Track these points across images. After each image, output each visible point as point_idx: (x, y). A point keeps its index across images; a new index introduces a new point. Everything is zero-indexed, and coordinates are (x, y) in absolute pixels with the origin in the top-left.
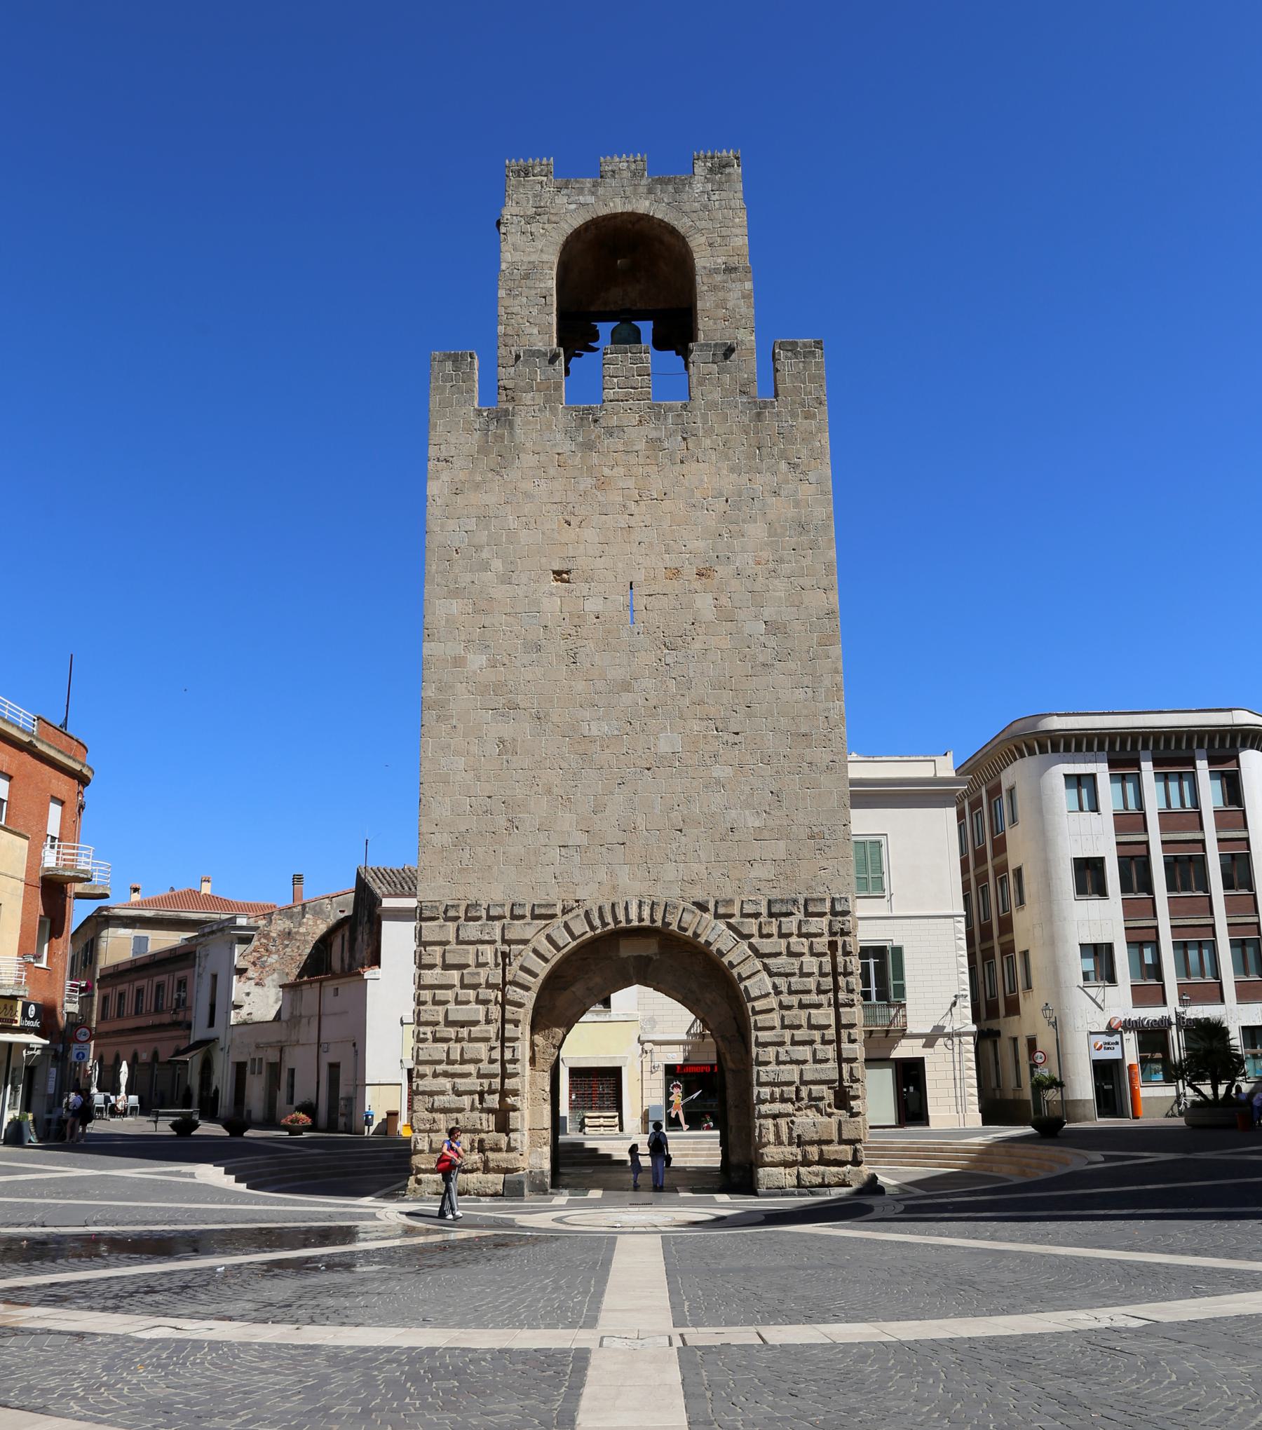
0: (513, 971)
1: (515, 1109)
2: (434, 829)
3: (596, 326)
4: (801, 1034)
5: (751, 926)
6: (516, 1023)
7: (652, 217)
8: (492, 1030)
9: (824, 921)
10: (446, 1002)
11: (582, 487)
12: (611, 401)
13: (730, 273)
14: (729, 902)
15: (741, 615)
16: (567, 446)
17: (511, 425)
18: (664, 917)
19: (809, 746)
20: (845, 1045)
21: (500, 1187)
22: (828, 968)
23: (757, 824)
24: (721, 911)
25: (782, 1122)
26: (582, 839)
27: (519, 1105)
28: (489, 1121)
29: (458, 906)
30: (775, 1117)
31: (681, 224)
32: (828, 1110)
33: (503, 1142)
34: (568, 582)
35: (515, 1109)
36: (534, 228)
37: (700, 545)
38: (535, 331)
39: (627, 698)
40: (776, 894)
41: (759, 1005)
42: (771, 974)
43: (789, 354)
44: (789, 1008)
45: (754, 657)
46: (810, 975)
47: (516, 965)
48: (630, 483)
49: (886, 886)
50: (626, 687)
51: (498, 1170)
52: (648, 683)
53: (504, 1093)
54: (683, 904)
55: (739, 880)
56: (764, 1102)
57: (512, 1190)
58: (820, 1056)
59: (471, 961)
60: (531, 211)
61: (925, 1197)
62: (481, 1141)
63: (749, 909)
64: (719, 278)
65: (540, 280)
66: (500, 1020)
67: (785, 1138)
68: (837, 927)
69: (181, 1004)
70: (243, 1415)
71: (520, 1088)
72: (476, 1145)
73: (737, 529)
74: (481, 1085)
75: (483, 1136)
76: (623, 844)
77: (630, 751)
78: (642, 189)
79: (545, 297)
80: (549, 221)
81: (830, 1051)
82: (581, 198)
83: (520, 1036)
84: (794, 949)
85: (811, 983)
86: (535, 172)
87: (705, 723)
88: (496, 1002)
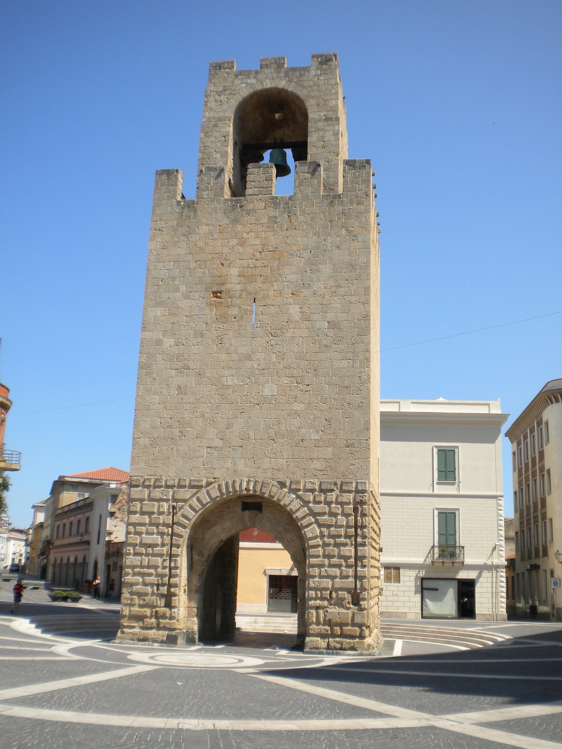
0: (179, 518)
1: (175, 595)
2: (141, 435)
4: (335, 560)
5: (310, 497)
6: (178, 546)
8: (165, 550)
9: (352, 495)
10: (142, 533)
11: (231, 244)
12: (250, 195)
14: (298, 482)
15: (315, 317)
16: (226, 221)
18: (261, 489)
19: (349, 394)
20: (359, 569)
21: (165, 638)
22: (352, 523)
24: (293, 486)
25: (321, 612)
26: (218, 443)
27: (177, 592)
29: (150, 479)
30: (317, 608)
31: (302, 93)
32: (348, 605)
33: (168, 613)
34: (220, 298)
35: (175, 595)
36: (223, 98)
37: (293, 277)
39: (248, 364)
40: (325, 479)
41: (311, 543)
43: (351, 167)
44: (328, 545)
45: (320, 341)
46: (341, 526)
47: (179, 514)
48: (258, 242)
49: (457, 477)
50: (248, 357)
51: (165, 628)
52: (261, 356)
53: (170, 586)
55: (304, 469)
56: (312, 599)
57: (171, 640)
58: (344, 573)
59: (156, 511)
60: (221, 89)
62: (156, 612)
63: (309, 486)
64: (321, 124)
65: (223, 127)
66: (169, 544)
67: (322, 620)
68: (358, 499)
69: (87, 532)
71: (178, 583)
72: (154, 614)
73: (316, 268)
74: (158, 580)
75: (158, 609)
76: (241, 447)
77: (248, 394)
78: (282, 74)
79: (225, 137)
80: (230, 94)
81: (351, 572)
83: (180, 553)
84: (334, 510)
85: (342, 531)
87: (291, 379)
88: (168, 535)
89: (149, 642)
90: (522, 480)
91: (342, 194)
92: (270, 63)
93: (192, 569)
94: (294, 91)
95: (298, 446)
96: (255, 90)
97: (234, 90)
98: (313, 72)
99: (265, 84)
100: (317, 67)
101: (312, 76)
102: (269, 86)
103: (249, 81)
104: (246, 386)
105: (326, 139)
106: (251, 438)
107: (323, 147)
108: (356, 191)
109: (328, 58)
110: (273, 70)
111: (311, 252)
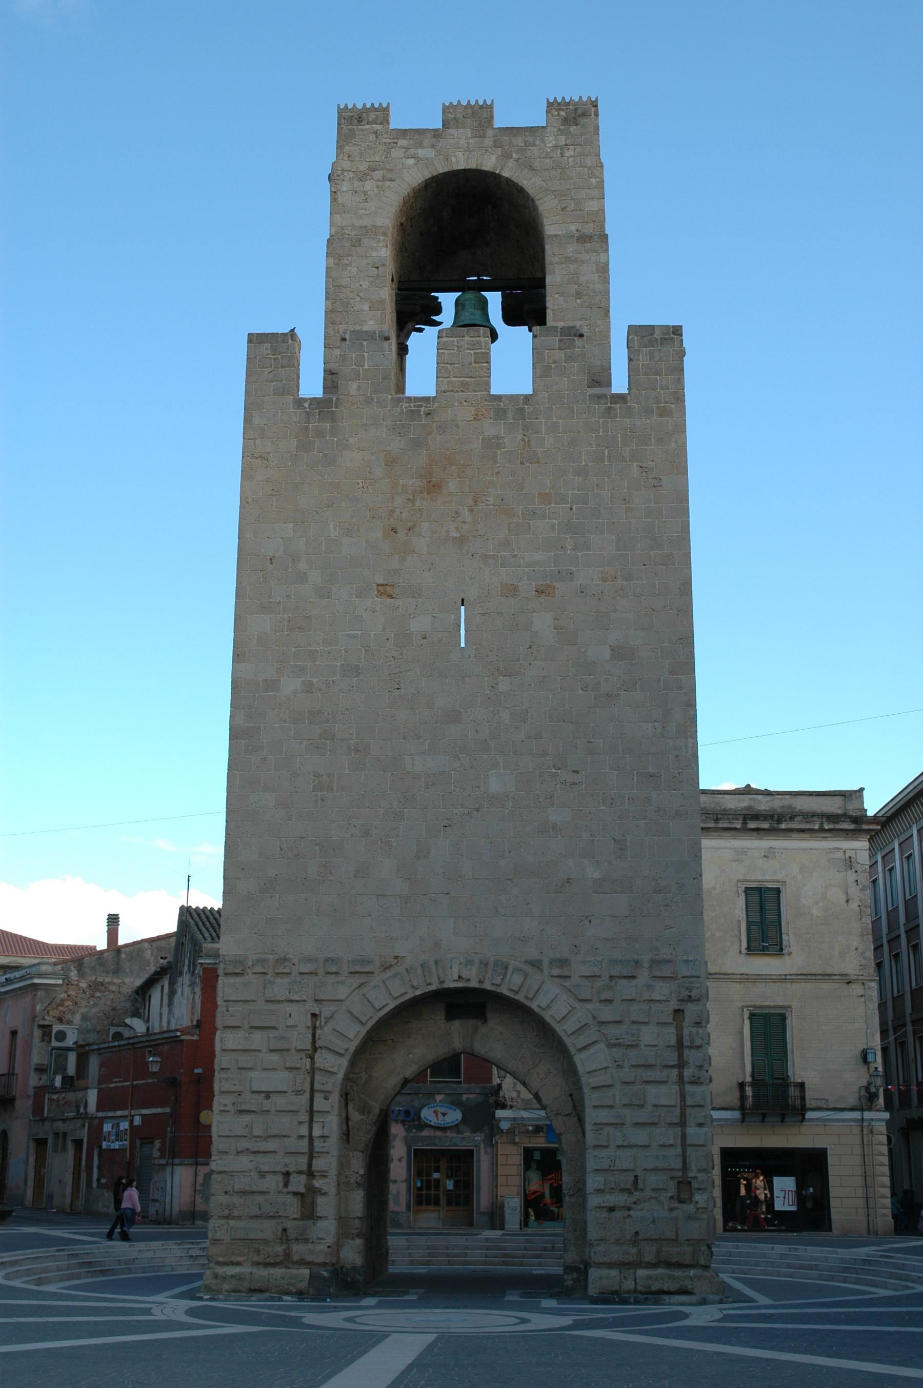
3: (437, 298)
7: (499, 175)
13: (585, 242)
17: (333, 418)
20: (691, 1130)
23: (597, 875)
28: (293, 1208)
31: (529, 183)
36: (369, 185)
38: (366, 307)
42: (611, 1046)
51: (302, 1263)
54: (513, 964)
61: (773, 1307)
65: (372, 248)
70: (117, 1082)
78: (488, 142)
82: (420, 151)
86: (370, 119)
89: (271, 1292)
90: (899, 936)
91: (629, 394)
92: (464, 116)
93: (348, 1141)
94: (513, 179)
95: (560, 892)
96: (435, 174)
97: (391, 170)
98: (550, 141)
99: (454, 160)
100: (559, 129)
101: (549, 147)
102: (462, 166)
103: (421, 152)
104: (452, 772)
105: (583, 279)
106: (467, 877)
107: (578, 295)
108: (657, 389)
109: (580, 112)
110: (468, 132)
111: (571, 509)
